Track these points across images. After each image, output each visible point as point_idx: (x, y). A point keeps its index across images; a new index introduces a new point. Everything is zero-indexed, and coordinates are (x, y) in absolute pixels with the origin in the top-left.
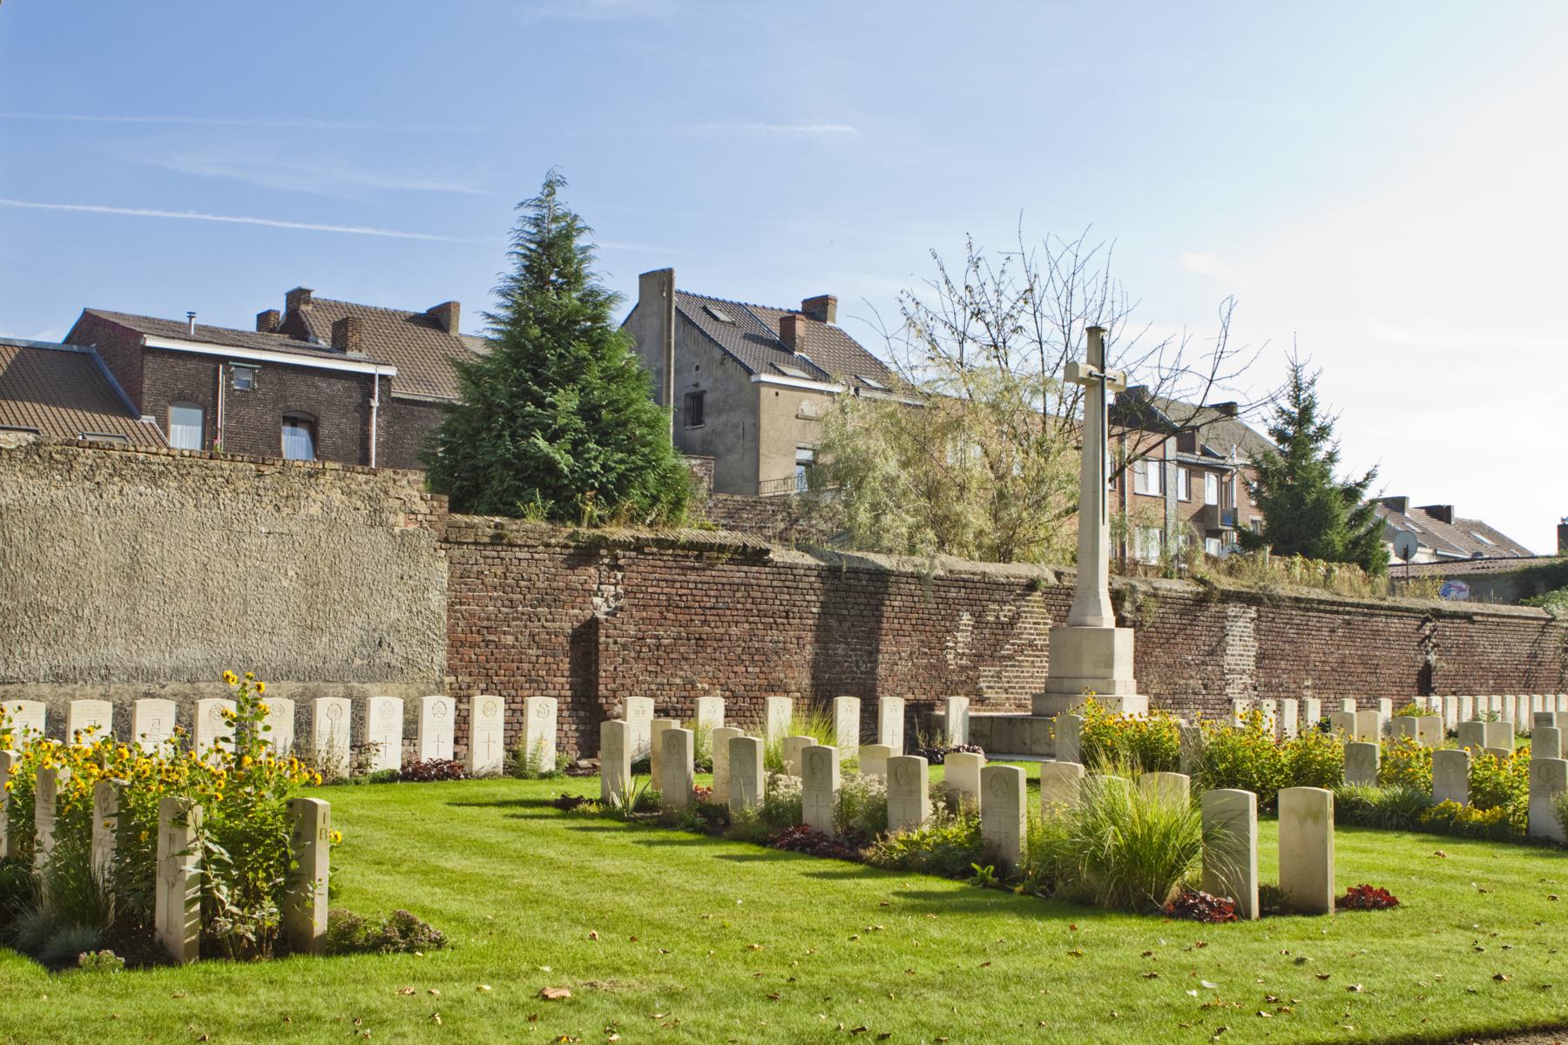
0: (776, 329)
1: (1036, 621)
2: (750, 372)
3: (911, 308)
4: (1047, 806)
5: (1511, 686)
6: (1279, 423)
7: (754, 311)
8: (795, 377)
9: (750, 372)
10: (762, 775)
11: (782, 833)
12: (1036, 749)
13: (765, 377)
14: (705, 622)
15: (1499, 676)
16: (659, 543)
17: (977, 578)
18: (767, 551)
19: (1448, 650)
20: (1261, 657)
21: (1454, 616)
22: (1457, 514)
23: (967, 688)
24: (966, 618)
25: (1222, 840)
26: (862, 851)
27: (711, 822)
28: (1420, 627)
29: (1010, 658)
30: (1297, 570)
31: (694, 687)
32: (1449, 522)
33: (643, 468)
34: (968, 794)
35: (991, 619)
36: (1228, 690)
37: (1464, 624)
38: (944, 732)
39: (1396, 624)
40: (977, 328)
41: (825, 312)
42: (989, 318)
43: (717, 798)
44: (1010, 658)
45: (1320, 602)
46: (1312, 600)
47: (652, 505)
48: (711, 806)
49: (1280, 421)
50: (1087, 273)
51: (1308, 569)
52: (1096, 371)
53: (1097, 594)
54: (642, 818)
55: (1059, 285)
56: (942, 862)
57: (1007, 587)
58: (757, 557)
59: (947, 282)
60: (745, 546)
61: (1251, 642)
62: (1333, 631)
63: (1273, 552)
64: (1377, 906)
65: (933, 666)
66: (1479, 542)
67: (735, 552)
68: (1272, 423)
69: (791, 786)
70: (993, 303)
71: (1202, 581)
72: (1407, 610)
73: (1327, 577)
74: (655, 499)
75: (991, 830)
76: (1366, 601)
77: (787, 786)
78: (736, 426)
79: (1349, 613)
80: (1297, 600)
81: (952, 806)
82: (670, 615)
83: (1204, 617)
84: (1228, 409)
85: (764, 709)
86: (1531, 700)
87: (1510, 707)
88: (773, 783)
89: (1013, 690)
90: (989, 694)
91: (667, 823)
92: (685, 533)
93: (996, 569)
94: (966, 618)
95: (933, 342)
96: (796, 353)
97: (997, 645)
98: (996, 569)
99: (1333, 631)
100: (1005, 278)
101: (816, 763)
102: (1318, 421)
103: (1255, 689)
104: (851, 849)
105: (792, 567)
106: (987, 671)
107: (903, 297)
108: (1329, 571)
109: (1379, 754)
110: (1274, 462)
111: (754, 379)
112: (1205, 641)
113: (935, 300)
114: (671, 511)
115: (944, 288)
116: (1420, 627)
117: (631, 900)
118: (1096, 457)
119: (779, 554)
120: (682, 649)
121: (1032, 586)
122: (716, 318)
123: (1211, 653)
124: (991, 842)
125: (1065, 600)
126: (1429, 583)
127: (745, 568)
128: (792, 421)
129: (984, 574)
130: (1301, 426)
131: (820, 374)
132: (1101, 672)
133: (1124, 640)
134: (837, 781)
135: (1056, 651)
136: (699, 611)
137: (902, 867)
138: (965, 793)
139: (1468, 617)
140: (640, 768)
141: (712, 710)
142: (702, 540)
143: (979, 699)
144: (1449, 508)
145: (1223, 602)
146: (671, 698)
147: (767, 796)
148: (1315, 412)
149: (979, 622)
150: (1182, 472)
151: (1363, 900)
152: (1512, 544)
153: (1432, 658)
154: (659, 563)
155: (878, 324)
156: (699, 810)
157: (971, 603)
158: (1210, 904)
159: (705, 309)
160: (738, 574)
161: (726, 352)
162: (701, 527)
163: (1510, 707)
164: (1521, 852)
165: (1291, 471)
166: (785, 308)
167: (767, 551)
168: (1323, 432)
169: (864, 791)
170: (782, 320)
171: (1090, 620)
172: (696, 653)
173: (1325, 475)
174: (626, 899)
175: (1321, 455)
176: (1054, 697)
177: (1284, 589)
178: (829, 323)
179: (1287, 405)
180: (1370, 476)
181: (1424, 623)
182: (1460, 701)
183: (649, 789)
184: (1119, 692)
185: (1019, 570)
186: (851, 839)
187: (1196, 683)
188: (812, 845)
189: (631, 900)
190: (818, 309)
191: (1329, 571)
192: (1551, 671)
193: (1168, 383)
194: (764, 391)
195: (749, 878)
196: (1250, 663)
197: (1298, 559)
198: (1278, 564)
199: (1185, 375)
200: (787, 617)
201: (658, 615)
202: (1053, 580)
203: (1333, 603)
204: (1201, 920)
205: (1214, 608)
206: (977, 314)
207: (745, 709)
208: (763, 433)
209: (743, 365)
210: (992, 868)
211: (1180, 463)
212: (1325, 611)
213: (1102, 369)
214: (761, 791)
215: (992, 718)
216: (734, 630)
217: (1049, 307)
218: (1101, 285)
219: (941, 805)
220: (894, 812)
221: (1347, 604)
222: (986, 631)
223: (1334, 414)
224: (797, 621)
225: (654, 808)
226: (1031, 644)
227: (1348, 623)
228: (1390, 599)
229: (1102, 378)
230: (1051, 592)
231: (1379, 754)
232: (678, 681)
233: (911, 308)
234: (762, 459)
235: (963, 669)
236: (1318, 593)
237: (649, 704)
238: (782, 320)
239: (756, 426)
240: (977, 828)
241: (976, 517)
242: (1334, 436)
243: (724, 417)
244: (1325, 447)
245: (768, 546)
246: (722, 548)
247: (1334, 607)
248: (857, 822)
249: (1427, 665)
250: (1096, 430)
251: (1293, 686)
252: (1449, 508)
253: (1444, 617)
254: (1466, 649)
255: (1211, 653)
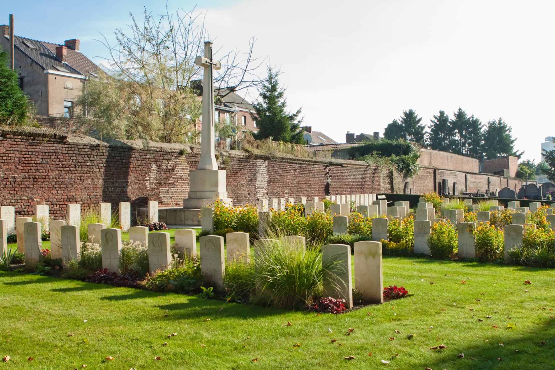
0: (54, 52)
1: (183, 168)
2: (44, 69)
3: (120, 37)
4: (236, 256)
5: (355, 191)
6: (264, 91)
7: (44, 44)
8: (63, 72)
9: (44, 69)
10: (79, 244)
11: (91, 274)
12: (186, 222)
13: (50, 71)
14: (37, 170)
15: (352, 187)
16: (15, 133)
17: (158, 149)
18: (66, 137)
19: (335, 177)
20: (269, 182)
21: (337, 164)
22: (313, 130)
23: (155, 197)
24: (154, 167)
25: (332, 270)
26: (139, 282)
27: (51, 269)
28: (325, 169)
29: (173, 184)
30: (282, 147)
31: (33, 200)
32: (310, 132)
33: (5, 97)
34: (189, 250)
35: (164, 167)
36: (258, 195)
37: (341, 168)
38: (147, 216)
39: (317, 168)
40: (148, 47)
41: (75, 46)
42: (154, 42)
43: (55, 254)
44: (173, 184)
45: (291, 159)
46: (287, 159)
47: (10, 115)
48: (50, 259)
49: (264, 90)
50: (194, 26)
51: (285, 146)
52: (209, 61)
53: (210, 156)
54: (15, 268)
55: (183, 29)
56: (181, 285)
57: (171, 153)
58: (62, 140)
59: (136, 26)
60: (55, 135)
61: (266, 175)
62: (295, 171)
63: (273, 140)
64: (398, 297)
65: (140, 188)
66: (321, 140)
67: (51, 137)
68: (261, 91)
69: (95, 248)
70: (155, 35)
71: (246, 151)
72: (321, 162)
73: (292, 149)
74: (12, 113)
75: (205, 268)
76: (307, 159)
77: (92, 249)
78: (38, 92)
79: (301, 164)
80: (282, 158)
81: (181, 256)
82: (20, 167)
83: (248, 166)
84: (232, 89)
85: (67, 211)
86: (351, 196)
87: (358, 199)
88: (84, 248)
89: (177, 196)
90: (164, 199)
91: (28, 270)
92: (28, 128)
93: (166, 146)
94: (154, 167)
95: (130, 52)
96: (63, 62)
97: (167, 178)
98: (166, 146)
99: (295, 171)
100: (161, 25)
101: (109, 237)
102: (279, 90)
103: (267, 194)
104: (133, 281)
105: (77, 145)
106: (163, 189)
107: (117, 31)
108: (293, 147)
109: (348, 221)
110: (262, 106)
111: (45, 72)
112: (249, 176)
113: (130, 34)
114: (19, 118)
115: (135, 28)
116: (325, 169)
117: (21, 325)
118: (209, 97)
119: (71, 139)
120: (26, 183)
121: (181, 153)
122: (28, 46)
123: (251, 180)
124: (207, 274)
125: (196, 161)
126: (327, 152)
127: (56, 145)
128: (63, 90)
129: (161, 148)
130: (271, 94)
131: (73, 71)
132: (213, 189)
133: (222, 175)
134: (120, 246)
135: (193, 181)
136: (34, 165)
137: (161, 289)
138: (187, 249)
139: (341, 165)
140: (12, 239)
141: (43, 211)
142: (34, 132)
143: (161, 202)
144: (310, 128)
145: (255, 159)
146: (22, 206)
147: (82, 253)
148: (277, 87)
149: (159, 169)
150: (217, 112)
151: (395, 294)
152: (332, 140)
153: (329, 181)
154: (14, 143)
155: (106, 43)
156: (45, 262)
157: (156, 160)
158: (335, 303)
159: (23, 42)
160: (52, 147)
161: (33, 61)
162: (34, 126)
163: (358, 199)
164: (411, 261)
165: (269, 109)
166: (57, 44)
167: (66, 137)
168: (281, 95)
169: (134, 249)
170: (57, 48)
171: (208, 167)
172: (33, 185)
173: (281, 111)
174: (19, 325)
175: (279, 104)
176: (193, 200)
177: (279, 155)
178: (76, 51)
179: (267, 84)
180: (299, 112)
181: (326, 167)
182: (341, 197)
183: (17, 252)
184: (221, 197)
185: (176, 146)
186: (132, 276)
187: (246, 193)
188: (111, 280)
189: (21, 325)
190: (71, 44)
191: (293, 147)
192: (368, 185)
193: (230, 70)
194: (50, 76)
195: (85, 303)
196: (265, 184)
197: (281, 142)
198: (274, 144)
199: (235, 68)
200: (75, 167)
201: (14, 167)
202: (189, 151)
203: (295, 160)
204: (332, 313)
205: (252, 162)
206: (149, 41)
207: (59, 212)
208: (50, 95)
209: (41, 66)
210: (212, 288)
211: (216, 109)
212: (292, 163)
213: (211, 60)
214: (79, 250)
215: (167, 210)
216: (51, 174)
217: (179, 39)
218: (200, 31)
219: (176, 255)
220: (152, 260)
221: (300, 160)
222: (162, 173)
223: (285, 88)
224: (80, 169)
225: (20, 261)
226: (181, 178)
227: (300, 167)
228: (314, 158)
229: (211, 64)
230: (189, 156)
231: (348, 221)
232: (25, 198)
233: (120, 37)
234: (50, 105)
235: (153, 189)
236: (289, 156)
237: (12, 209)
238: (57, 48)
239: (47, 92)
240: (198, 267)
241: (156, 123)
242: (284, 97)
243: (33, 88)
244: (281, 100)
245: (66, 135)
246: (44, 136)
247: (295, 161)
248: (133, 266)
249: (328, 184)
250: (209, 86)
251: (281, 193)
252: (310, 128)
253: (333, 165)
254: (340, 177)
255: (251, 180)
